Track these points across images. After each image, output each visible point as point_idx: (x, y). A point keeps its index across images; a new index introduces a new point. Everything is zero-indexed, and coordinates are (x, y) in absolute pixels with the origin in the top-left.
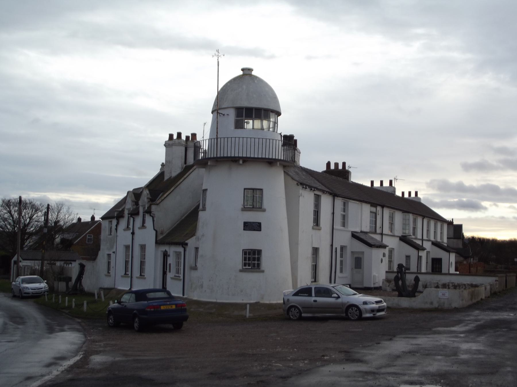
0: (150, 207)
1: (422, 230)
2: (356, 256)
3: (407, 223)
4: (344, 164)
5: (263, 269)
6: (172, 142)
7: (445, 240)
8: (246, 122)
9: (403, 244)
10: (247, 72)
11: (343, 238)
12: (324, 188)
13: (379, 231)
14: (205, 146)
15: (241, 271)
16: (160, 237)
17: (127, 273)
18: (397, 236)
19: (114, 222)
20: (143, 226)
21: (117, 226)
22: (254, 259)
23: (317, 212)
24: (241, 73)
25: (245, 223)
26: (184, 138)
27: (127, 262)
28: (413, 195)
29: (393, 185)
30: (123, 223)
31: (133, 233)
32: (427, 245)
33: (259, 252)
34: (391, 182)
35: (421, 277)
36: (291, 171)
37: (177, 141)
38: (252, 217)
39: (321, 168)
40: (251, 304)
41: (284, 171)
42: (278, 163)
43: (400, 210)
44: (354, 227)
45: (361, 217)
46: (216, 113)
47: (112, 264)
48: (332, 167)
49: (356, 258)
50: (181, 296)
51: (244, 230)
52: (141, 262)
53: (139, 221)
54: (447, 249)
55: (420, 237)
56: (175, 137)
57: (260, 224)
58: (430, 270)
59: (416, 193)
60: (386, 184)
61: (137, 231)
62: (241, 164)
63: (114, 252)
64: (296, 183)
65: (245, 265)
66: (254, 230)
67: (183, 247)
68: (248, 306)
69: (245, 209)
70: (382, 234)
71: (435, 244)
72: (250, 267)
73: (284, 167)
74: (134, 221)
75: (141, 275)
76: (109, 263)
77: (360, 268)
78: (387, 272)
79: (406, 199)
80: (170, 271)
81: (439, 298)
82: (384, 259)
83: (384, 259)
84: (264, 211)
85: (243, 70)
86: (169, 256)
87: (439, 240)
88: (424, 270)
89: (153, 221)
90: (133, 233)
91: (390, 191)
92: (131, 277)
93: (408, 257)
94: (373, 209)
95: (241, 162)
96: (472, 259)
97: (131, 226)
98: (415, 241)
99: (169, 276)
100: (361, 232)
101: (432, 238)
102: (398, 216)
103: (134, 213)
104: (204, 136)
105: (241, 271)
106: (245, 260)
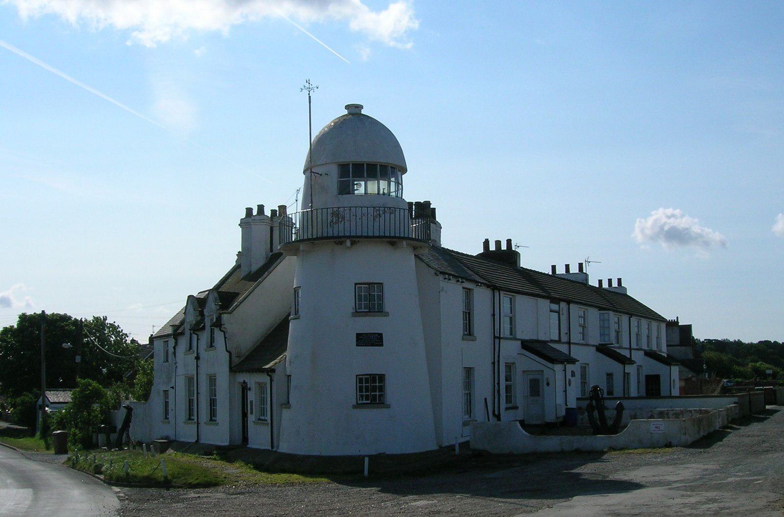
0: (219, 318)
1: (626, 333)
2: (531, 377)
3: (606, 325)
4: (509, 242)
5: (41, 312)
6: (251, 220)
7: (664, 348)
8: (357, 184)
9: (600, 355)
10: (354, 110)
11: (510, 350)
12: (478, 279)
13: (564, 338)
14: (297, 221)
15: (354, 407)
16: (236, 361)
17: (192, 418)
18: (593, 346)
19: (172, 342)
20: (211, 345)
21: (174, 348)
22: (374, 389)
23: (469, 313)
24: (346, 112)
25: (358, 335)
26: (268, 213)
27: (190, 402)
28: (615, 284)
29: (584, 271)
30: (183, 342)
31: (198, 358)
32: (638, 356)
33: (382, 378)
34: (581, 265)
35: (626, 403)
36: (425, 252)
37: (258, 218)
38: (368, 324)
39: (475, 249)
40: (371, 457)
41: (415, 255)
42: (404, 243)
43: (596, 307)
44: (525, 332)
45: (536, 319)
46: (308, 172)
47: (171, 406)
48: (492, 247)
49: (531, 381)
50: (270, 448)
51: (357, 345)
52: (211, 399)
53: (205, 337)
54: (668, 361)
55: (626, 344)
56: (255, 213)
57: (380, 336)
58: (643, 392)
59: (619, 280)
60: (574, 269)
61: (203, 354)
62: (348, 248)
63: (173, 388)
64: (433, 271)
65: (362, 396)
66: (373, 345)
67: (268, 375)
68: (367, 460)
69: (357, 313)
70: (569, 343)
71: (650, 354)
72: (369, 402)
73: (415, 248)
74: (198, 339)
75: (211, 420)
76: (167, 404)
77: (538, 395)
78: (578, 399)
79: (605, 290)
80: (252, 413)
81: (651, 433)
82: (572, 379)
83: (572, 379)
84: (387, 314)
85: (347, 107)
86: (250, 389)
87: (654, 348)
88: (633, 392)
89: (225, 338)
90: (198, 358)
91: (580, 279)
92: (198, 423)
93: (610, 376)
94: (555, 307)
95: (348, 243)
96: (707, 375)
97: (195, 348)
98: (618, 351)
99: (251, 418)
100: (537, 341)
101: (645, 347)
102: (593, 314)
103: (197, 328)
104: (295, 210)
105: (354, 407)
106: (361, 391)
